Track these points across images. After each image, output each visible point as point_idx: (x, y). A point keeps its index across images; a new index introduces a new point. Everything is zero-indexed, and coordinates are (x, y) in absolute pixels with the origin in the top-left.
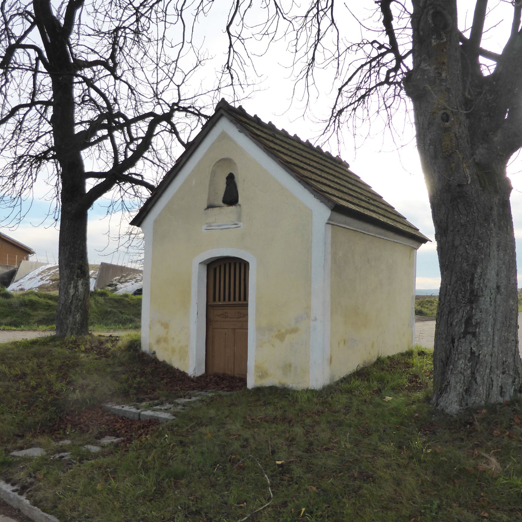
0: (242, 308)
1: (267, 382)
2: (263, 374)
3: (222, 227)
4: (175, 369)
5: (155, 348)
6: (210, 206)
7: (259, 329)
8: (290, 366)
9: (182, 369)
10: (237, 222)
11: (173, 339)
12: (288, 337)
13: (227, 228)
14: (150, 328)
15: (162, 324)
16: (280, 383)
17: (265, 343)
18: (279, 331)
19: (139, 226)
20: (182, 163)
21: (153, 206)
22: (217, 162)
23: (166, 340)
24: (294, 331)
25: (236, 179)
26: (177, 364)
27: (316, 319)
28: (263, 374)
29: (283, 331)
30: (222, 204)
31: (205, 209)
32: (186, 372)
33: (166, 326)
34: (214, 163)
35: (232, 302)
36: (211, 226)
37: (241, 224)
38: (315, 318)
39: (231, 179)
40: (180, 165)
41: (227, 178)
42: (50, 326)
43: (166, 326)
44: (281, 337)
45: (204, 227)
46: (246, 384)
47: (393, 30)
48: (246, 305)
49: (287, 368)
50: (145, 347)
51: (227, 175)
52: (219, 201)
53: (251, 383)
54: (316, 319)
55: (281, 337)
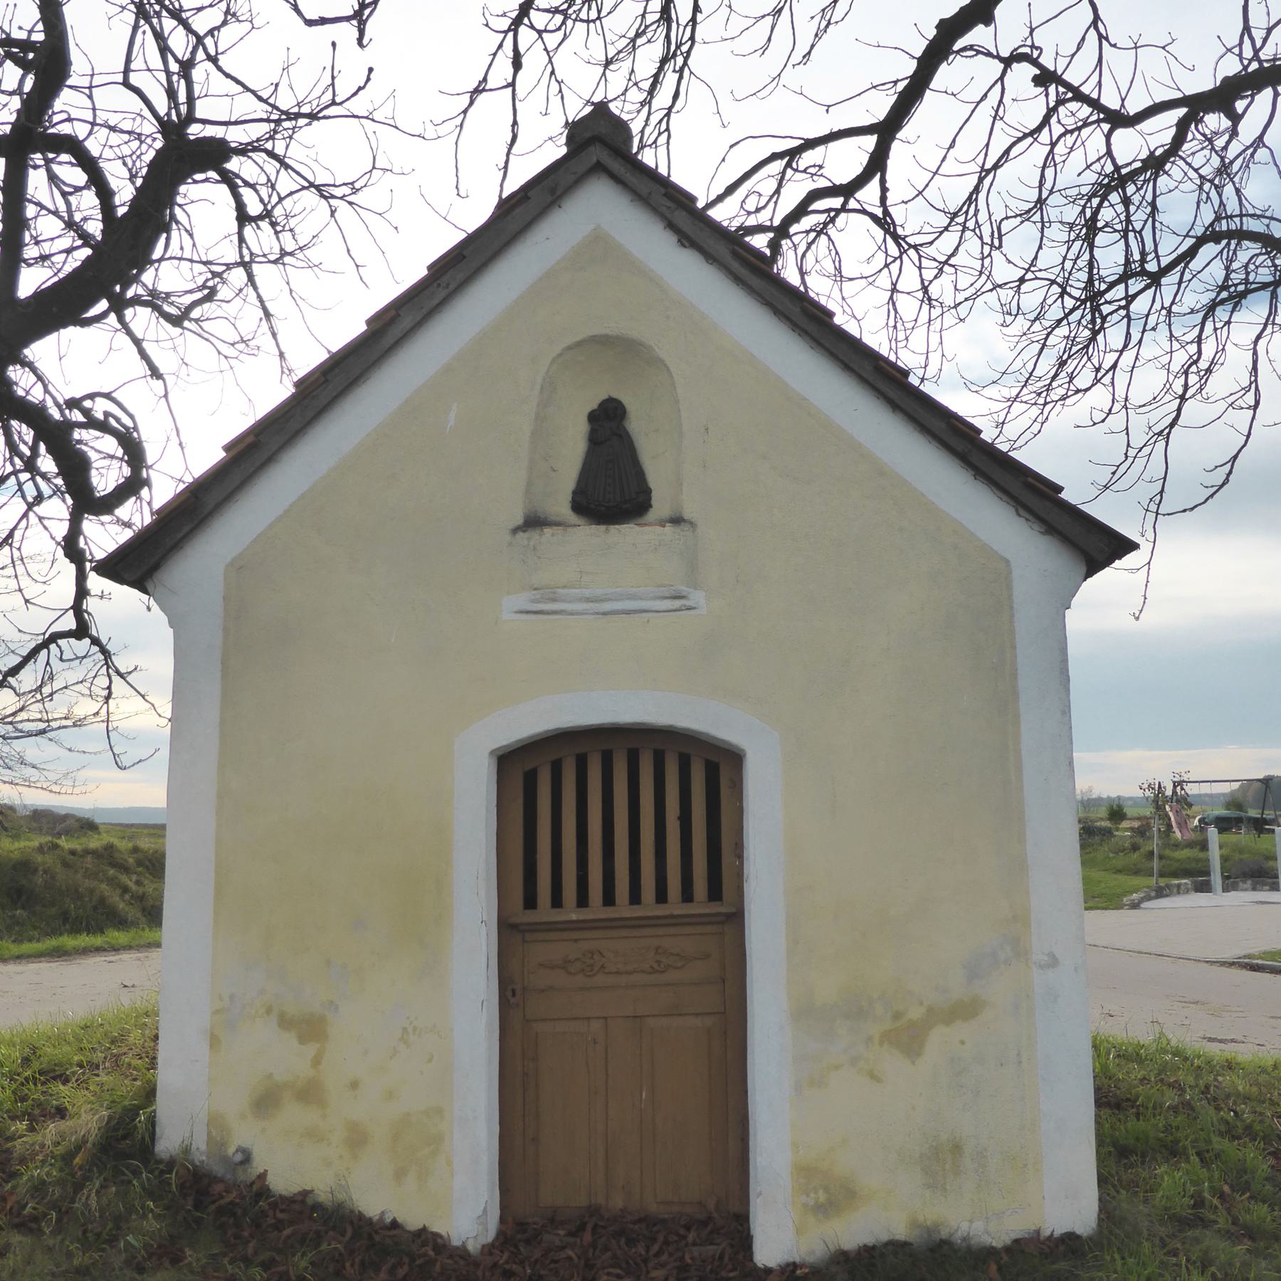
0: (672, 930)
1: (855, 1230)
2: (829, 1194)
3: (607, 606)
4: (370, 1222)
5: (243, 1134)
6: (534, 522)
7: (805, 1013)
8: (957, 1148)
9: (412, 1218)
10: (684, 589)
11: (354, 1085)
12: (938, 1037)
13: (628, 612)
14: (214, 1042)
15: (285, 1022)
16: (914, 1224)
17: (837, 1067)
18: (897, 1016)
19: (140, 584)
20: (396, 331)
21: (228, 498)
22: (569, 348)
23: (310, 1093)
24: (965, 1010)
25: (636, 425)
26: (377, 1196)
27: (1053, 962)
28: (829, 1194)
29: (916, 1013)
30: (572, 517)
31: (515, 531)
32: (436, 1227)
33: (310, 1029)
34: (557, 349)
35: (572, 914)
36: (554, 600)
37: (697, 597)
38: (1052, 956)
39: (608, 422)
40: (388, 340)
41: (593, 417)
42: (89, 1145)
43: (310, 1029)
44: (909, 1039)
45: (523, 600)
46: (745, 1242)
47: (919, 59)
48: (736, 918)
49: (942, 1159)
50: (179, 1127)
51: (594, 405)
52: (561, 506)
53: (776, 1237)
54: (1053, 962)
55: (909, 1039)
